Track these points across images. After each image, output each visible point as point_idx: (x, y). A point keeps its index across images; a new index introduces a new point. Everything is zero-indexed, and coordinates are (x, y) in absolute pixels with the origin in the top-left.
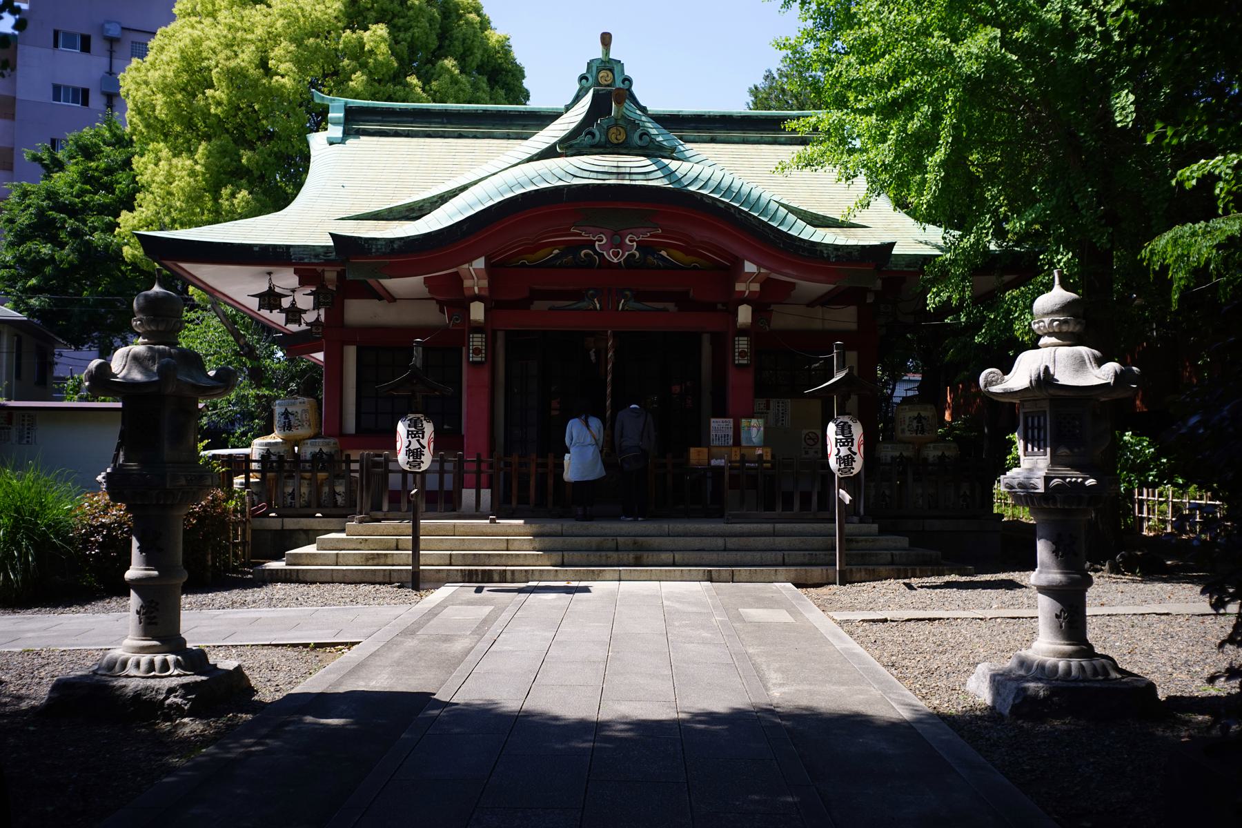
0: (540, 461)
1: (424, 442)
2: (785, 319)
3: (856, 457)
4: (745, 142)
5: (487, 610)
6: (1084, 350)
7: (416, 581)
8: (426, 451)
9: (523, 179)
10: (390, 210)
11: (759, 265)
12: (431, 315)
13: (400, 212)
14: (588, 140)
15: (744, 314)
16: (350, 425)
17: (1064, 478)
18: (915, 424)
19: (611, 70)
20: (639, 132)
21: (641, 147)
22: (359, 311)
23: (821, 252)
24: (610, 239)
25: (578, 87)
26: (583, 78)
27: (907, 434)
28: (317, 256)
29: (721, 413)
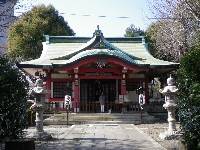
0: (91, 103)
1: (70, 100)
2: (131, 76)
3: (143, 102)
4: (123, 43)
5: (82, 128)
6: (174, 86)
7: (69, 125)
8: (70, 102)
9: (85, 54)
10: (60, 58)
11: (127, 68)
12: (67, 77)
13: (62, 58)
14: (96, 47)
15: (124, 76)
16: (52, 97)
17: (171, 105)
18: (157, 95)
19: (99, 32)
20: (105, 45)
21: (106, 48)
22: (54, 76)
23: (138, 66)
24: (101, 64)
25: (93, 35)
26: (94, 33)
27: (155, 97)
28: (48, 67)
29: (120, 93)
